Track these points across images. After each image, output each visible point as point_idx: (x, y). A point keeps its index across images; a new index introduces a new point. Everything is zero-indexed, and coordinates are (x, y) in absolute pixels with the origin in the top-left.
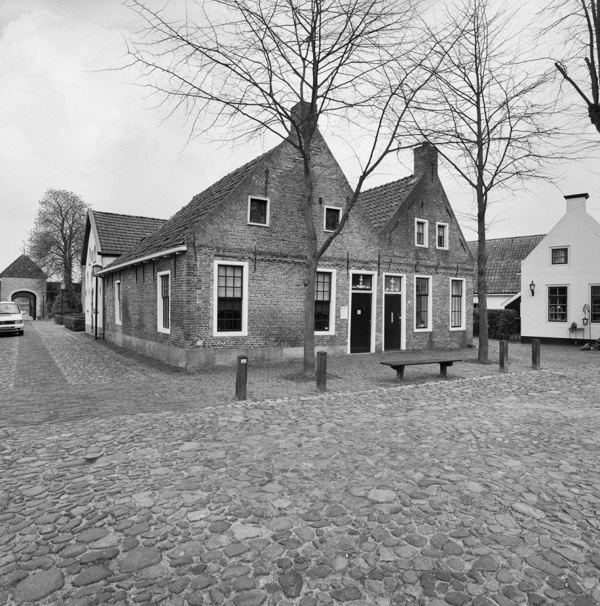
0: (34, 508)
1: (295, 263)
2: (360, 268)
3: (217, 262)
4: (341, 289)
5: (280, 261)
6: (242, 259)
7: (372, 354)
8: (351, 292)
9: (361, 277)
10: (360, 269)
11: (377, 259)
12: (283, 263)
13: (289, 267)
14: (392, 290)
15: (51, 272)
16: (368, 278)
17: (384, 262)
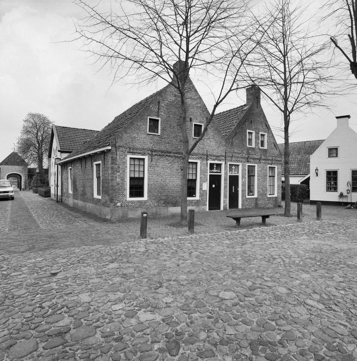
0: (20, 303)
1: (176, 157)
2: (214, 160)
3: (129, 156)
4: (203, 172)
5: (167, 155)
6: (144, 154)
7: (222, 211)
8: (209, 174)
9: (215, 165)
10: (214, 160)
11: (224, 154)
12: (169, 157)
13: (172, 159)
14: (233, 172)
15: (31, 162)
16: (219, 166)
17: (229, 156)
